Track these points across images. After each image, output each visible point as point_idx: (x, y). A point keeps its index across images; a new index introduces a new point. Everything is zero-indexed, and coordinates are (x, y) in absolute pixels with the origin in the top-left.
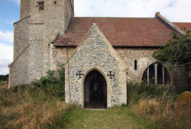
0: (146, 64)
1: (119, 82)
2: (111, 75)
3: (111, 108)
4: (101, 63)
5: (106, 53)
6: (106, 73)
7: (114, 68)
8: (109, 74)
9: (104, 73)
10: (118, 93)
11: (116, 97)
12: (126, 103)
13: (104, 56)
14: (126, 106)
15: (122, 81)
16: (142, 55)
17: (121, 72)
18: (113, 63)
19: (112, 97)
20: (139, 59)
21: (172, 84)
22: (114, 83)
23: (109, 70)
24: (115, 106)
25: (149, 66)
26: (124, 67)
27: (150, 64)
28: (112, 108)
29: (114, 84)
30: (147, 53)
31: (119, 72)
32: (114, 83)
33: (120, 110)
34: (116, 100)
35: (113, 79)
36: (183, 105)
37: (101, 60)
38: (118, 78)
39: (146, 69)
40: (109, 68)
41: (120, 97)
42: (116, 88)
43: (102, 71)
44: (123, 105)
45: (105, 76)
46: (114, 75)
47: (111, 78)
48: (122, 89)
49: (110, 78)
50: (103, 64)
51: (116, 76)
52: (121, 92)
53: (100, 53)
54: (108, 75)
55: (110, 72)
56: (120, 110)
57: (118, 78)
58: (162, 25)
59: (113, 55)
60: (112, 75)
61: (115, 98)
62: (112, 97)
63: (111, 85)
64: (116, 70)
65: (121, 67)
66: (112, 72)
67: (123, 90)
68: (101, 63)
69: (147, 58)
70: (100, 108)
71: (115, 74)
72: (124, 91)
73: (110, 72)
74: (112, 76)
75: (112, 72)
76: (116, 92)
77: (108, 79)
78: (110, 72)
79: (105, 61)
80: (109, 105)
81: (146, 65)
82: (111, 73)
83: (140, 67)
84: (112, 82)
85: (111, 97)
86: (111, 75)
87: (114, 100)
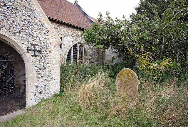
0: (71, 43)
1: (49, 63)
2: (35, 51)
3: (34, 107)
4: (14, 26)
5: (26, 10)
6: (24, 46)
7: (42, 39)
8: (31, 48)
9: (21, 45)
10: (46, 78)
11: (43, 86)
12: (58, 93)
13: (20, 14)
14: (59, 95)
15: (53, 60)
16: (67, 34)
17: (51, 48)
18: (39, 31)
19: (37, 87)
20: (64, 36)
21: (88, 62)
22: (41, 63)
23: (31, 41)
24: (43, 101)
25: (73, 46)
26: (57, 40)
27: (75, 44)
28: (38, 106)
29: (40, 66)
30: (72, 33)
31: (49, 46)
32: (41, 63)
33: (51, 106)
34: (43, 90)
35: (38, 58)
36: (125, 83)
37: (12, 19)
38: (46, 55)
39: (70, 50)
40: (31, 37)
41: (50, 84)
42: (44, 71)
43: (16, 41)
44: (56, 95)
45: (20, 52)
46: (40, 51)
47: (35, 56)
48: (53, 72)
49: (33, 55)
50: (19, 28)
51: (45, 52)
52: (51, 77)
53: (10, 3)
54: (29, 50)
55: (32, 45)
56: (51, 106)
57: (46, 55)
58: (80, 13)
59: (40, 17)
60: (38, 51)
61: (42, 88)
62: (37, 87)
63: (36, 68)
64: (43, 43)
65: (53, 40)
66: (37, 45)
67: (54, 74)
68: (14, 26)
69: (72, 37)
70: (12, 110)
71: (43, 50)
72: (57, 75)
73: (32, 45)
74: (37, 53)
75: (37, 45)
76: (43, 78)
77: (29, 59)
78: (34, 45)
79: (23, 23)
80: (31, 100)
81: (71, 45)
82: (34, 47)
83: (66, 46)
84: (37, 63)
85: (35, 88)
86: (35, 51)
87: (41, 92)
